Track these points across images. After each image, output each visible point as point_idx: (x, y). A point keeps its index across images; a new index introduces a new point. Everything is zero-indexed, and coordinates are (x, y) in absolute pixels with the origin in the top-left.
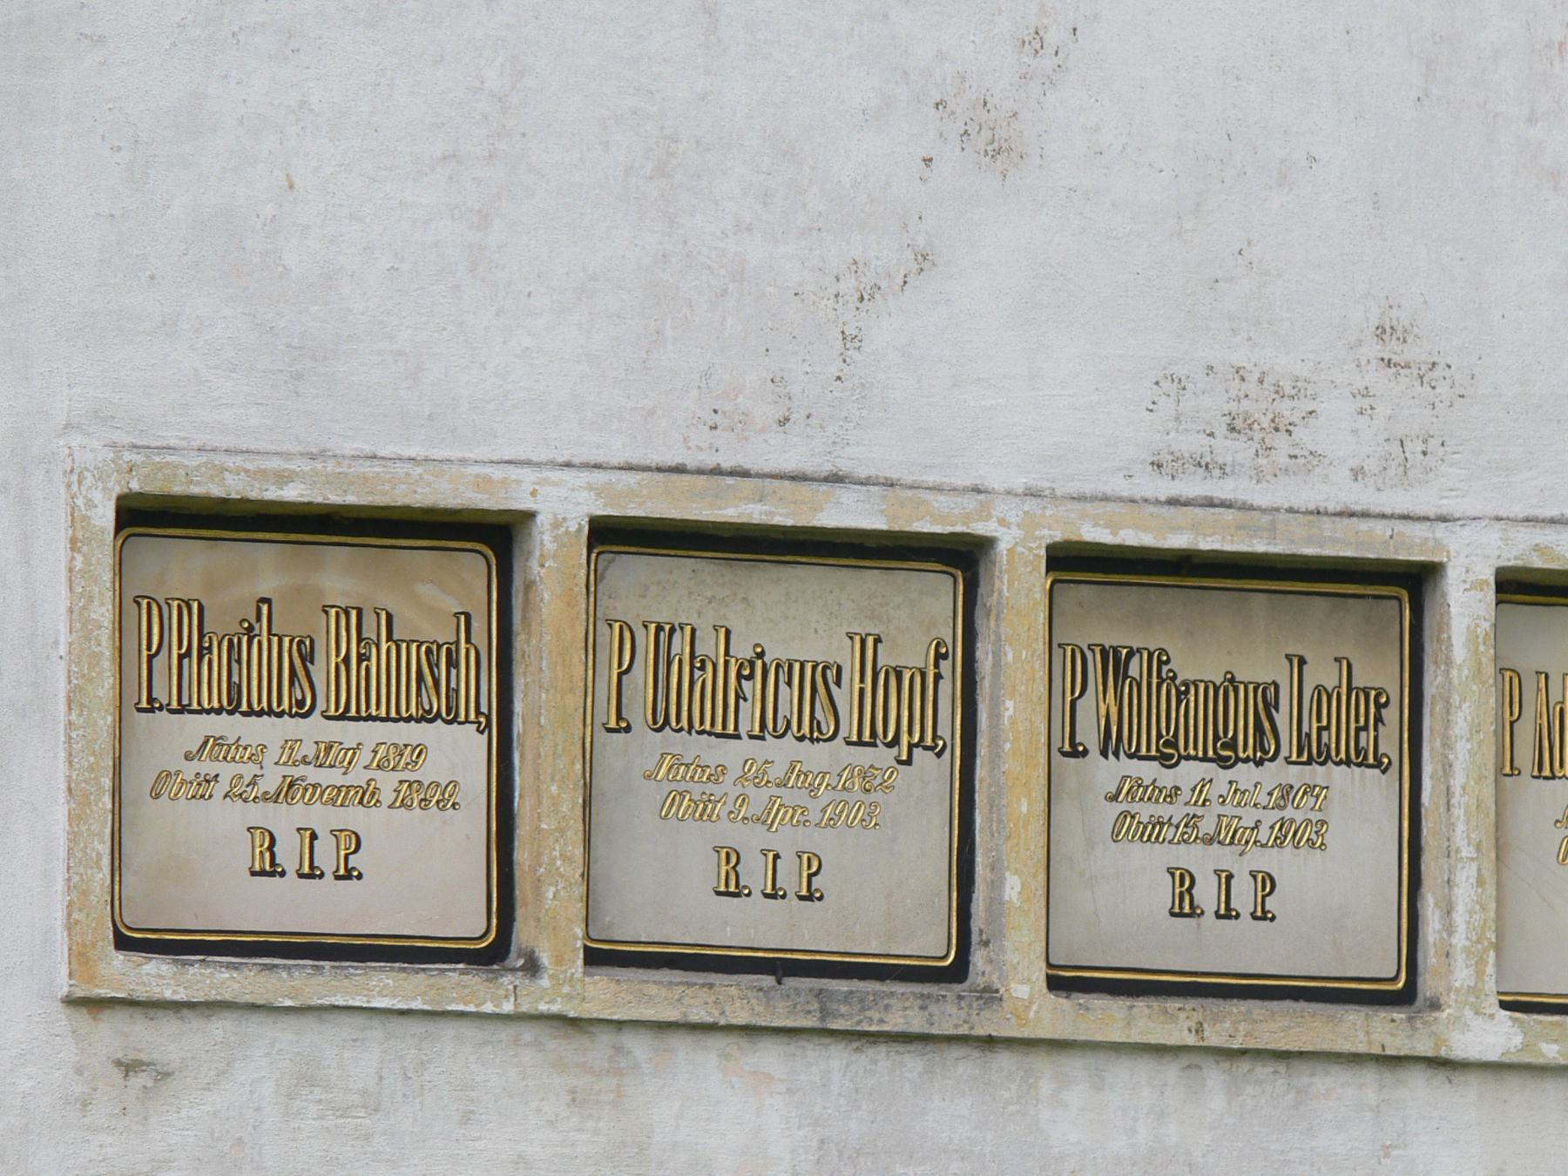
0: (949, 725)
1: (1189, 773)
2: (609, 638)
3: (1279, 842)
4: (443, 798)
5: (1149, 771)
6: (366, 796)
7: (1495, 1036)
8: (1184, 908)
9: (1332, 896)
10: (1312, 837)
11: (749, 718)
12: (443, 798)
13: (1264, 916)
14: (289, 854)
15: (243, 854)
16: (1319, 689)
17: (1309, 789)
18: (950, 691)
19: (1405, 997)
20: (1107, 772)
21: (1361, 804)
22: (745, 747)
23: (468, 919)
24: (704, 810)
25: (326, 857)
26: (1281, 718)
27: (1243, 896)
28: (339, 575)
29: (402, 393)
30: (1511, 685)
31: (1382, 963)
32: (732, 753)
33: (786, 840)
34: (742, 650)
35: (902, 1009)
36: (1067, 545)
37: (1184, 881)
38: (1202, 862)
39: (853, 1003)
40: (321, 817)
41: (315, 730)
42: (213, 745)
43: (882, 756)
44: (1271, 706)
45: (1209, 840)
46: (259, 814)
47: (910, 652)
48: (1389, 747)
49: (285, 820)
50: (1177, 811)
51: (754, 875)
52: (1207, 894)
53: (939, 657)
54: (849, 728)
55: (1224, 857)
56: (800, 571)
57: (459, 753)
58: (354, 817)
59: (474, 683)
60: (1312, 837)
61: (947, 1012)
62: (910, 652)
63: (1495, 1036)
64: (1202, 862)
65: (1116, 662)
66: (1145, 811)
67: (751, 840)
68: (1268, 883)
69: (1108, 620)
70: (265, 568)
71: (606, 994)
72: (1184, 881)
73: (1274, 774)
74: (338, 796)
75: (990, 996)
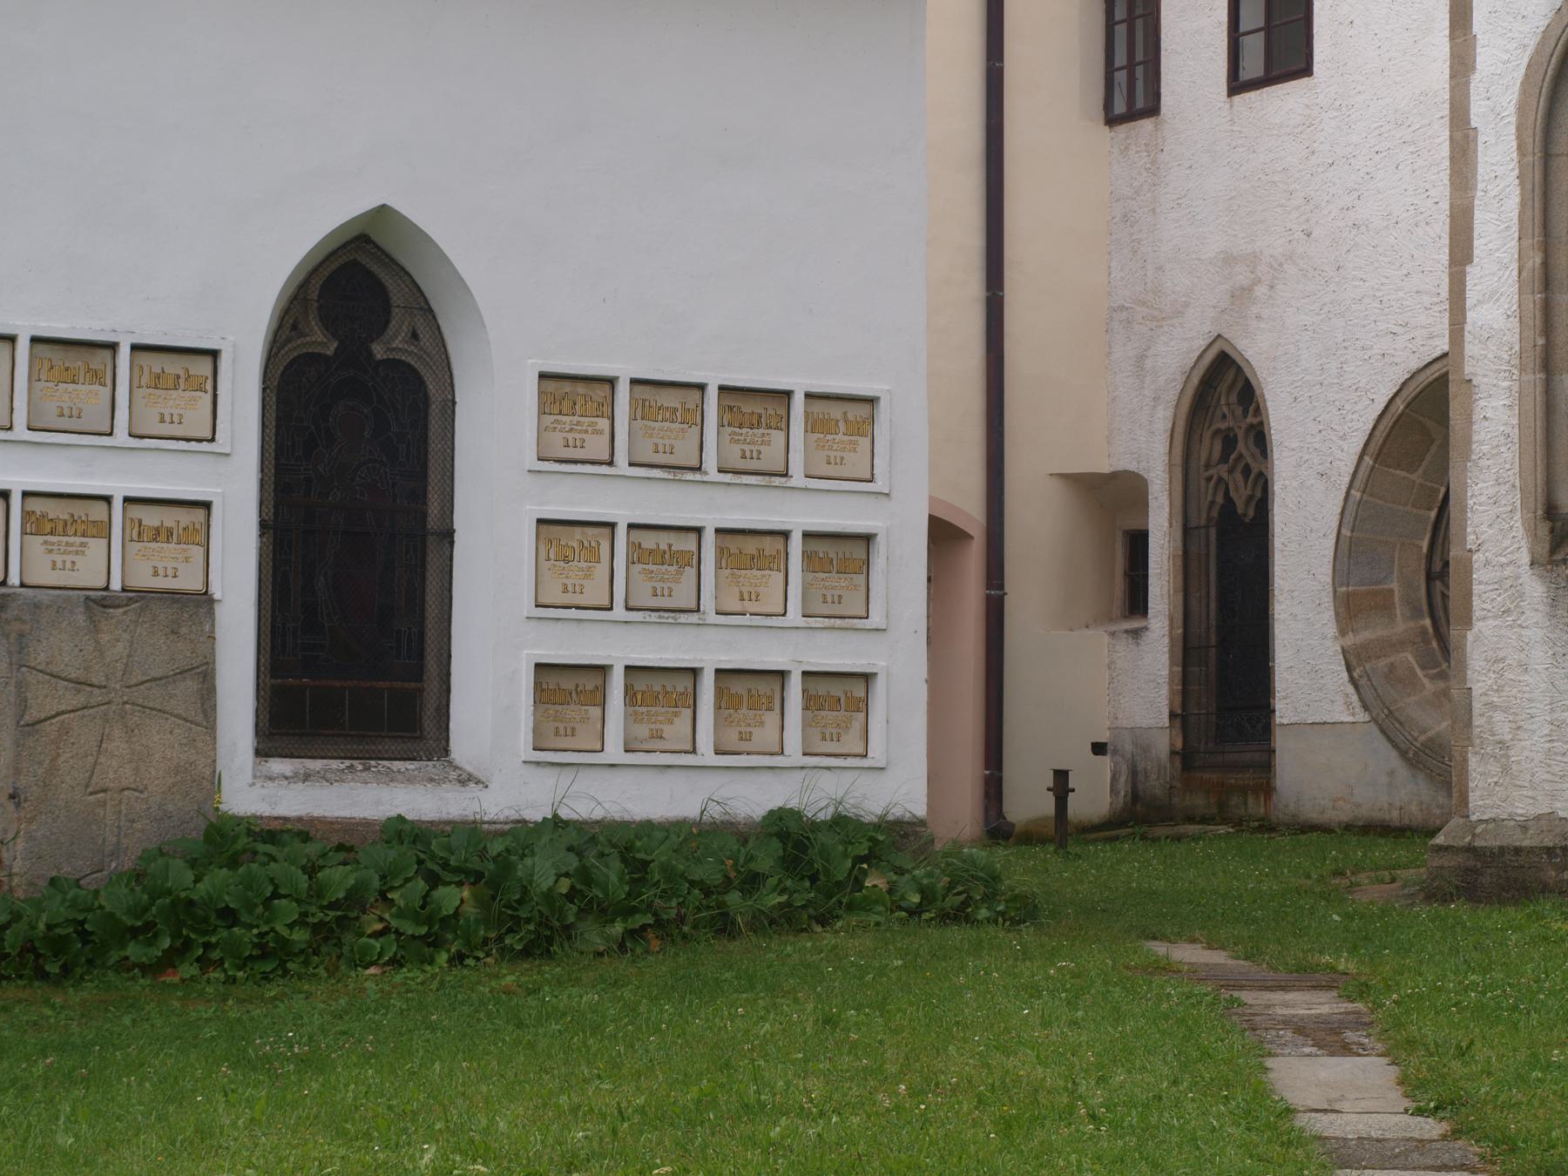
1: (744, 431)
4: (600, 432)
6: (586, 432)
7: (802, 622)
8: (156, 574)
12: (600, 432)
14: (571, 443)
15: (562, 443)
19: (786, 475)
20: (729, 430)
21: (778, 437)
23: (606, 457)
24: (651, 436)
27: (68, 565)
33: (667, 442)
35: (690, 476)
38: (747, 448)
40: (577, 436)
41: (576, 418)
42: (578, 423)
49: (570, 436)
51: (661, 448)
63: (802, 622)
64: (747, 448)
65: (731, 408)
67: (660, 442)
68: (759, 452)
72: (744, 451)
73: (761, 431)
75: (706, 473)
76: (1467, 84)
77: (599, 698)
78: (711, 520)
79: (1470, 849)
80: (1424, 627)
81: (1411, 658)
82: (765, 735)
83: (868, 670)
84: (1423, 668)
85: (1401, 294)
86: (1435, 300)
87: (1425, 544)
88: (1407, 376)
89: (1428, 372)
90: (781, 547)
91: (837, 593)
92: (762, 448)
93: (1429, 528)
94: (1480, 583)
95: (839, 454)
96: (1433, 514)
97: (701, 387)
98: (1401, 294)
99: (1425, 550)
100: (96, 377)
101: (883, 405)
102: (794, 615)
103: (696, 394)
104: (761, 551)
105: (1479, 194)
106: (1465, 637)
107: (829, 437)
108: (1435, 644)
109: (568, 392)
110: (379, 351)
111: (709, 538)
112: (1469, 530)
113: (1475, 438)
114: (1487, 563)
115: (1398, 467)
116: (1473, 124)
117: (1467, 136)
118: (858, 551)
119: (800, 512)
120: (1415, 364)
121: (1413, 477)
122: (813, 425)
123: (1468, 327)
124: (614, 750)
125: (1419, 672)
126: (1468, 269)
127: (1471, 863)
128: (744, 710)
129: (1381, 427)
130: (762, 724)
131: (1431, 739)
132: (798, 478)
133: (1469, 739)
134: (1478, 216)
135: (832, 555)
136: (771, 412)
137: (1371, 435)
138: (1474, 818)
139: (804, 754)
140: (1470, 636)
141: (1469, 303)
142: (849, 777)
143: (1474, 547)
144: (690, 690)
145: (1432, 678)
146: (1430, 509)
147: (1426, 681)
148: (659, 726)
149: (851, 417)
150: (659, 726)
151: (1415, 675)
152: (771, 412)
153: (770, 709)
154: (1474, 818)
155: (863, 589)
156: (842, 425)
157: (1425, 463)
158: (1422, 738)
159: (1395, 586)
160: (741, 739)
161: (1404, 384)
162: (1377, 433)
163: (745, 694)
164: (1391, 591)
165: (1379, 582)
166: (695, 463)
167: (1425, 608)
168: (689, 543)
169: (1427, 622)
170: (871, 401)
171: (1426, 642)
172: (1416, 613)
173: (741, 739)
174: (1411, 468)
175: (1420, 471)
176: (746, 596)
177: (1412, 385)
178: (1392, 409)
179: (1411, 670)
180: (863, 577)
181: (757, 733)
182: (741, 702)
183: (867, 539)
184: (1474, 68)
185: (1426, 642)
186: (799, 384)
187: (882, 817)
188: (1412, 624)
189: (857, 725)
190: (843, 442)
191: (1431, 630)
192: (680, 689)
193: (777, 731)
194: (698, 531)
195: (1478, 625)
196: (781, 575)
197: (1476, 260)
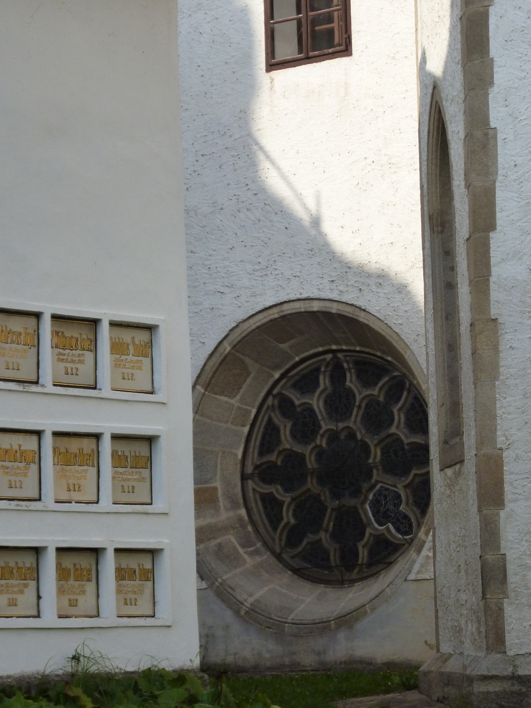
3: (78, 362)
5: (62, 351)
10: (81, 362)
11: (9, 341)
13: (77, 375)
15: (63, 371)
16: (83, 338)
17: (83, 355)
18: (36, 337)
22: (9, 345)
25: (74, 372)
26: (78, 343)
29: (220, 270)
32: (8, 345)
34: (8, 329)
36: (54, 314)
44: (77, 341)
45: (70, 362)
48: (92, 348)
50: (65, 357)
52: (69, 371)
53: (35, 331)
54: (22, 343)
56: (15, 317)
61: (34, 388)
64: (69, 365)
66: (61, 357)
72: (66, 368)
73: (78, 352)
76: (486, 95)
77: (35, 574)
78: (49, 424)
79: (515, 678)
80: (240, 515)
81: (233, 540)
82: (86, 601)
83: (158, 547)
84: (243, 546)
85: (227, 263)
86: (257, 267)
87: (240, 453)
88: (234, 325)
89: (251, 321)
90: (94, 447)
91: (131, 483)
92: (79, 366)
93: (243, 440)
94: (511, 473)
95: (130, 371)
96: (246, 429)
97: (37, 315)
98: (227, 263)
99: (240, 456)
101: (162, 332)
102: (106, 502)
103: (32, 321)
104: (81, 450)
105: (500, 178)
106: (498, 514)
107: (123, 357)
108: (250, 528)
111: (48, 440)
112: (498, 433)
113: (502, 363)
114: (517, 458)
115: (222, 393)
116: (492, 125)
117: (486, 135)
118: (142, 449)
119: (109, 418)
120: (242, 315)
121: (232, 401)
122: (117, 348)
123: (492, 279)
124: (49, 617)
125: (241, 550)
126: (492, 235)
127: (516, 688)
128: (72, 582)
129: (211, 363)
130: (84, 592)
131: (257, 601)
132: (106, 391)
133: (504, 592)
134: (500, 195)
135: (127, 453)
136: (84, 336)
137: (203, 369)
138: (510, 653)
139: (60, 617)
140: (502, 514)
141: (493, 261)
142: (80, 636)
143: (504, 447)
144: (35, 565)
145: (251, 554)
146: (243, 426)
147: (246, 557)
148: (14, 596)
149: (137, 342)
150: (14, 596)
151: (238, 552)
152: (84, 336)
153: (89, 580)
154: (510, 653)
155: (148, 480)
156: (131, 348)
157: (242, 391)
158: (251, 600)
159: (218, 484)
160: (70, 605)
161: (231, 330)
162: (207, 368)
163: (71, 567)
164: (215, 489)
165: (206, 482)
166: (34, 378)
167: (241, 501)
168: (30, 444)
169: (243, 512)
170: (150, 329)
171: (243, 526)
172: (234, 505)
173: (70, 605)
174: (231, 396)
175: (238, 397)
176: (72, 488)
177: (238, 331)
178: (221, 350)
179: (235, 548)
180: (148, 471)
181: (81, 600)
182: (69, 575)
183: (150, 440)
184: (491, 83)
185: (243, 526)
186: (106, 313)
187: (164, 669)
188: (231, 514)
189: (148, 591)
190: (131, 361)
191: (246, 518)
192: (28, 565)
193: (95, 597)
194: (39, 433)
195: (509, 506)
196: (95, 470)
197: (498, 228)
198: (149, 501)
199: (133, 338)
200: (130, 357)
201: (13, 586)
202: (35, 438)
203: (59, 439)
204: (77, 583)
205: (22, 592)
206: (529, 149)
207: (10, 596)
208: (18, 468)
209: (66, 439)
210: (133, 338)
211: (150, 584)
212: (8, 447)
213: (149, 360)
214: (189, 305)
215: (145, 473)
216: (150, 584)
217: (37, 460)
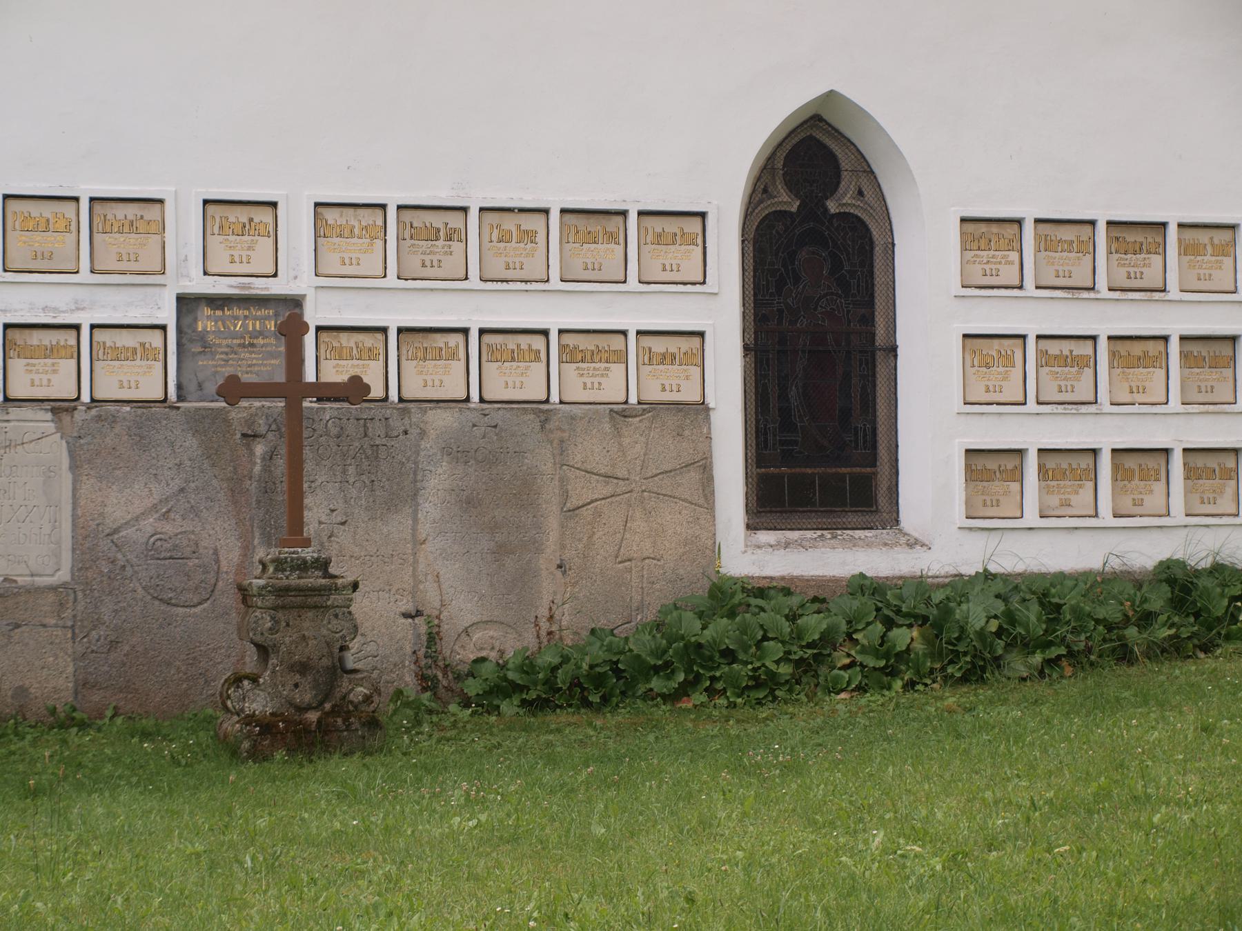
0: (1091, 250)
1: (1129, 256)
2: (401, 225)
4: (1012, 263)
6: (1000, 263)
9: (1152, 276)
10: (1149, 266)
12: (1012, 263)
15: (981, 273)
19: (1164, 291)
20: (1116, 256)
21: (1157, 260)
24: (1053, 264)
28: (994, 228)
30: (1180, 240)
31: (1161, 285)
33: (1066, 268)
35: (1085, 295)
37: (1129, 273)
38: (1132, 270)
39: (1078, 294)
40: (993, 267)
41: (992, 253)
42: (976, 256)
43: (577, 245)
46: (423, 257)
47: (1085, 238)
49: (987, 267)
51: (1061, 274)
52: (1132, 275)
55: (430, 257)
57: (1014, 256)
58: (998, 266)
59: (1016, 245)
60: (1149, 266)
62: (1085, 238)
64: (1132, 270)
65: (1117, 239)
67: (1060, 268)
68: (1142, 273)
69: (1116, 232)
70: (983, 228)
71: (402, 284)
72: (1129, 273)
73: (1143, 256)
74: (995, 263)
75: (1098, 292)
77: (1018, 475)
78: (1103, 330)
82: (1154, 500)
90: (1162, 349)
95: (1207, 272)
100: (611, 237)
104: (1146, 354)
107: (1199, 258)
109: (984, 232)
110: (832, 207)
111: (1103, 344)
124: (1031, 516)
128: (1136, 482)
132: (1174, 292)
136: (1150, 240)
142: (1223, 533)
144: (1092, 466)
148: (1067, 496)
149: (1216, 241)
150: (1067, 496)
152: (1150, 240)
153: (1158, 480)
155: (1231, 380)
160: (1135, 505)
166: (1090, 284)
176: (1135, 390)
180: (1231, 370)
181: (1147, 499)
186: (1173, 218)
190: (1210, 262)
192: (1083, 466)
194: (1094, 338)
196: (1163, 372)
198: (1232, 400)
199: (1212, 239)
200: (1207, 258)
201: (1065, 487)
202: (1090, 343)
203: (1112, 342)
204: (1142, 483)
205: (1077, 493)
206: (6, 418)
207: (1063, 497)
208: (1070, 373)
209: (1128, 343)
210: (1212, 239)
211: (1233, 483)
212: (1058, 353)
213: (1231, 259)
214: (425, 359)
215: (1228, 372)
216: (1233, 483)
217: (1092, 364)
